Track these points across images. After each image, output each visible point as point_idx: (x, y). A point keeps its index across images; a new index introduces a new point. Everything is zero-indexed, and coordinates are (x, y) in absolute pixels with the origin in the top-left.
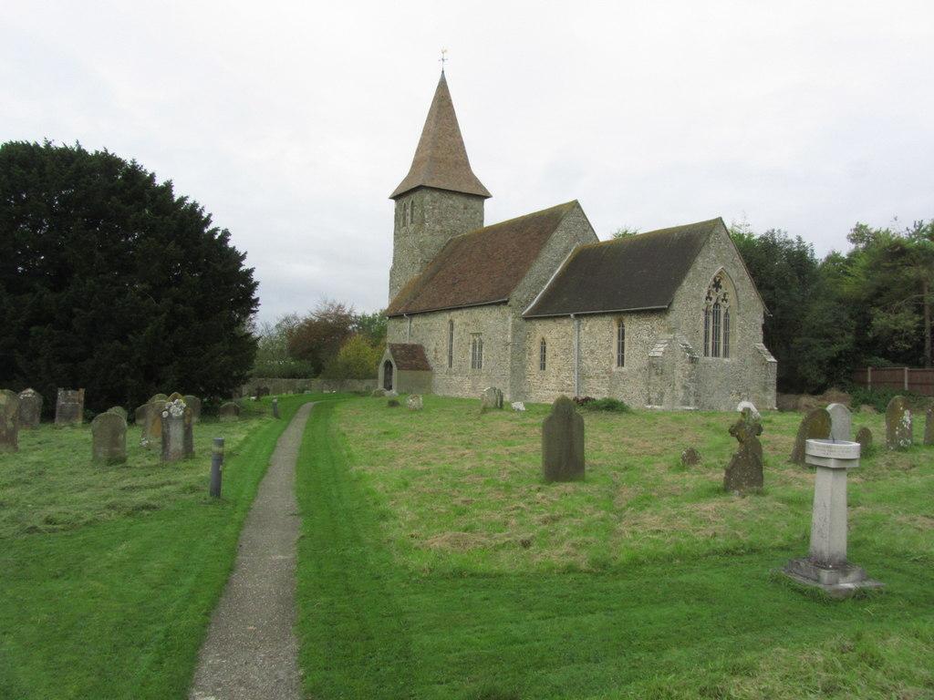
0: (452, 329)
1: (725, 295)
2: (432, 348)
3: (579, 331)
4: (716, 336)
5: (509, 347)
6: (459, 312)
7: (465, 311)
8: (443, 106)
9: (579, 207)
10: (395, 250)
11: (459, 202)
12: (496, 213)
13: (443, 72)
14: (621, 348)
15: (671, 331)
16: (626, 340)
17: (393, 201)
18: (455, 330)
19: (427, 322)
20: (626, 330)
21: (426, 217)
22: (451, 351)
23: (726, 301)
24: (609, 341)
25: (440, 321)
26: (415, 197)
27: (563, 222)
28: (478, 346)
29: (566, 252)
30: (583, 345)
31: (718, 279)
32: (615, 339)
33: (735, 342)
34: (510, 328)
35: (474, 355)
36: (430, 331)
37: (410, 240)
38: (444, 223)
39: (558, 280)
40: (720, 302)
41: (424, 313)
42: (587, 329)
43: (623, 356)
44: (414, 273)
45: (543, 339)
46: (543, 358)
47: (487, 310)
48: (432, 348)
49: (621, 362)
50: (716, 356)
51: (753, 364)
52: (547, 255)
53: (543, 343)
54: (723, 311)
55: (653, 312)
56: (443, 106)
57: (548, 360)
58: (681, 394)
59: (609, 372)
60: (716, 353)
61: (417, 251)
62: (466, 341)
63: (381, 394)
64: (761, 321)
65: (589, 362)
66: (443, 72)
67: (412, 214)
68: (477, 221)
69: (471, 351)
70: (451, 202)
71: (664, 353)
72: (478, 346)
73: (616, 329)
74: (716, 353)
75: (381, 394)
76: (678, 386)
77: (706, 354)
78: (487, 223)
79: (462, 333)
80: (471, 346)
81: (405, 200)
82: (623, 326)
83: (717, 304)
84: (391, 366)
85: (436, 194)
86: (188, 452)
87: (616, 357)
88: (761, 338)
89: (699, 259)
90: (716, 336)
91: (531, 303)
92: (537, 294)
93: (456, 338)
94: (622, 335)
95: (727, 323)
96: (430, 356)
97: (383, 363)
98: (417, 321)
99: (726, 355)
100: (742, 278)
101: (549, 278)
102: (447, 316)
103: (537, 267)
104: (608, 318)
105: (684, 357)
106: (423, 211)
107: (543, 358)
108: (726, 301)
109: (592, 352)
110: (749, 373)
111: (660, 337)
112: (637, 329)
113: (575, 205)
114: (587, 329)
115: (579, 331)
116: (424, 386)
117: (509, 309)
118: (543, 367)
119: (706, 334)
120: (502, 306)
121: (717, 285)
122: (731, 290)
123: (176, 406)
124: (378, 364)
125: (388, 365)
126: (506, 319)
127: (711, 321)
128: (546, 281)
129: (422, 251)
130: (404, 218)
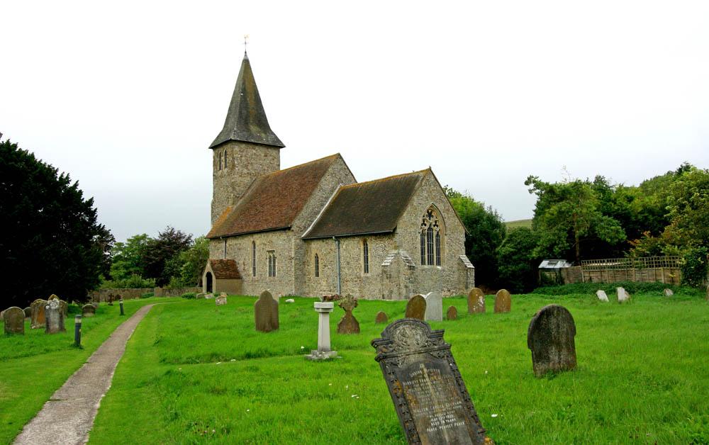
0: (255, 248)
1: (436, 222)
2: (241, 262)
4: (430, 251)
5: (293, 261)
6: (259, 235)
7: (263, 235)
8: (246, 63)
9: (341, 158)
10: (214, 188)
11: (260, 151)
12: (289, 159)
15: (396, 248)
16: (369, 254)
17: (212, 150)
18: (257, 248)
19: (237, 242)
22: (254, 265)
25: (246, 242)
26: (228, 148)
28: (272, 260)
29: (332, 191)
32: (362, 253)
33: (445, 253)
34: (293, 247)
35: (270, 266)
36: (240, 249)
38: (250, 167)
40: (432, 227)
41: (236, 236)
42: (344, 247)
44: (231, 207)
46: (317, 268)
47: (278, 234)
48: (241, 262)
49: (366, 270)
50: (431, 264)
52: (318, 194)
53: (317, 257)
54: (435, 233)
56: (246, 63)
57: (320, 270)
61: (230, 189)
62: (264, 256)
64: (463, 239)
65: (346, 270)
67: (226, 160)
68: (274, 165)
69: (268, 263)
70: (254, 151)
72: (272, 260)
73: (362, 247)
74: (431, 262)
77: (423, 263)
78: (282, 168)
80: (268, 260)
81: (220, 150)
83: (430, 229)
84: (211, 276)
85: (243, 146)
86: (62, 329)
87: (363, 266)
88: (464, 251)
89: (415, 198)
90: (430, 251)
94: (366, 251)
95: (438, 241)
96: (240, 268)
98: (231, 242)
99: (439, 263)
100: (448, 210)
103: (313, 202)
104: (357, 239)
105: (405, 265)
106: (233, 158)
107: (317, 268)
108: (437, 226)
109: (348, 263)
112: (373, 245)
113: (339, 156)
114: (344, 247)
115: (339, 248)
118: (317, 275)
120: (287, 231)
121: (430, 215)
122: (440, 218)
123: (54, 303)
124: (201, 274)
125: (209, 275)
126: (290, 240)
127: (426, 241)
128: (320, 212)
129: (234, 189)
130: (220, 163)
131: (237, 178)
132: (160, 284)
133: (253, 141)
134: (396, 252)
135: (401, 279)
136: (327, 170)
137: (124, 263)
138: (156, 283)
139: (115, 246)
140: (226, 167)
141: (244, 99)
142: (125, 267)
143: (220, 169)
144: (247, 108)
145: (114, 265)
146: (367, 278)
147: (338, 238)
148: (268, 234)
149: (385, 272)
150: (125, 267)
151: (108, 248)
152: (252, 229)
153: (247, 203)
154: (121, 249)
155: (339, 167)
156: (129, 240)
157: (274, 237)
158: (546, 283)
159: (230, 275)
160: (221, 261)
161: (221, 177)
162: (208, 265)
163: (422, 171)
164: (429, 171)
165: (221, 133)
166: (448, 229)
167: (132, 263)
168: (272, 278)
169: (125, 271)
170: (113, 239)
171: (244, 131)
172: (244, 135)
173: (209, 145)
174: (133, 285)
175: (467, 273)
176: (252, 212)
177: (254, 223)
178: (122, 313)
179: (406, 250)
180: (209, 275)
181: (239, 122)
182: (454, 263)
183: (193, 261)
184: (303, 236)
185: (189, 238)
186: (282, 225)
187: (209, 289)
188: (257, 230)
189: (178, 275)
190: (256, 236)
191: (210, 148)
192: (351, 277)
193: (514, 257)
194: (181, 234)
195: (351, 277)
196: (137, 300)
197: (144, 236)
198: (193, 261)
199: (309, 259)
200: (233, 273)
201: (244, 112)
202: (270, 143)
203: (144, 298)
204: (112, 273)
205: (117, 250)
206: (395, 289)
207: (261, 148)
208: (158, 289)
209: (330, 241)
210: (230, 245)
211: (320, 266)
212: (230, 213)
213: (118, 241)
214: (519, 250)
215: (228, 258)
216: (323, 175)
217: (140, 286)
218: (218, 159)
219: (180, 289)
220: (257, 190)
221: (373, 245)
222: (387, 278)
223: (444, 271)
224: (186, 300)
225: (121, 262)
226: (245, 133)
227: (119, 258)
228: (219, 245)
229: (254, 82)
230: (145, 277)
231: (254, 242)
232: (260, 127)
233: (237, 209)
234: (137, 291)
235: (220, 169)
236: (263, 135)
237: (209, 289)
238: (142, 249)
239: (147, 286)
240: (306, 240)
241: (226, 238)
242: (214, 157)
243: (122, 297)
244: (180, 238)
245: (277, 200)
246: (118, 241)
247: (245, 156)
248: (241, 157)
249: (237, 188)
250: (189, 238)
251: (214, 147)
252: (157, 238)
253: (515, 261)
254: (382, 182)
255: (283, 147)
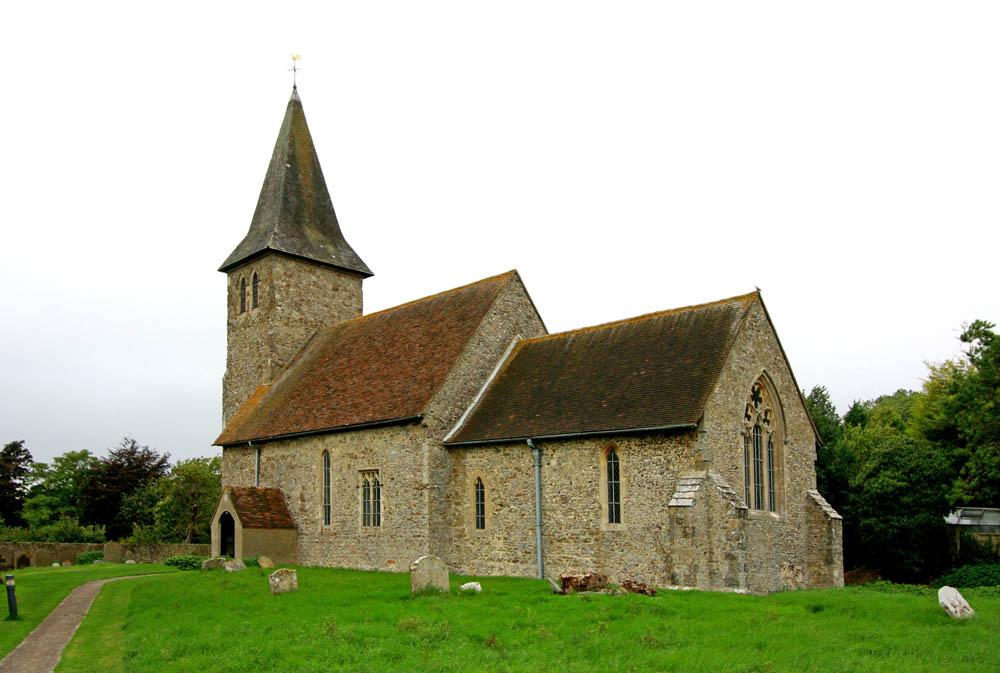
0: (328, 463)
2: (296, 494)
3: (540, 466)
5: (426, 492)
6: (340, 437)
7: (348, 436)
8: (295, 108)
9: (519, 280)
10: (230, 349)
11: (325, 279)
12: (378, 297)
13: (295, 87)
14: (614, 493)
15: (701, 465)
16: (622, 480)
17: (225, 275)
18: (334, 465)
20: (622, 465)
21: (277, 296)
22: (327, 499)
23: (768, 422)
24: (594, 482)
25: (308, 454)
26: (261, 268)
27: (498, 302)
28: (372, 492)
30: (548, 490)
31: (756, 387)
34: (425, 462)
35: (366, 505)
37: (254, 334)
38: (304, 308)
39: (495, 389)
40: (761, 423)
41: (283, 440)
42: (554, 463)
43: (618, 507)
44: (267, 384)
45: (479, 479)
46: (481, 509)
47: (386, 434)
48: (296, 494)
49: (615, 516)
50: (759, 509)
51: (808, 521)
52: (475, 352)
54: (765, 438)
55: (668, 434)
56: (295, 108)
58: (724, 568)
59: (595, 532)
60: (759, 505)
61: (265, 349)
62: (352, 482)
63: (217, 566)
65: (559, 516)
66: (295, 87)
67: (255, 293)
69: (360, 498)
70: (314, 278)
71: (695, 500)
72: (372, 492)
73: (603, 463)
75: (217, 566)
76: (718, 554)
78: (366, 312)
79: (345, 471)
80: (361, 490)
81: (244, 273)
82: (616, 458)
83: (757, 427)
85: (292, 265)
87: (605, 507)
89: (733, 353)
91: (455, 423)
92: (464, 410)
93: (334, 478)
94: (614, 473)
96: (294, 506)
97: (217, 517)
99: (772, 508)
101: (482, 385)
102: (319, 445)
103: (465, 367)
104: (589, 445)
105: (728, 506)
106: (272, 287)
107: (481, 509)
110: (802, 536)
111: (684, 474)
112: (630, 458)
113: (514, 277)
114: (554, 463)
115: (540, 466)
116: (287, 555)
117: (422, 431)
118: (481, 524)
119: (747, 469)
120: (410, 426)
122: (775, 406)
125: (227, 521)
126: (418, 447)
128: (478, 390)
130: (243, 300)
131: (282, 330)
132: (113, 535)
133: (311, 256)
134: (702, 474)
135: (714, 539)
136: (490, 304)
137: (48, 499)
138: (106, 535)
139: (31, 469)
140: (255, 306)
141: (293, 174)
142: (51, 506)
143: (243, 311)
144: (298, 194)
145: (29, 501)
146: (619, 534)
147: (539, 443)
148: (361, 434)
149: (679, 521)
150: (51, 506)
151: (20, 472)
152: (321, 425)
153: (304, 376)
154: (43, 475)
155: (517, 299)
156: (57, 460)
157: (376, 441)
158: (981, 556)
159: (272, 519)
160: (253, 491)
161: (246, 325)
162: (226, 498)
163: (736, 299)
164: (756, 298)
165: (243, 242)
166: (789, 431)
167: (62, 500)
168: (371, 529)
169: (50, 512)
170: (28, 457)
171: (293, 236)
172: (294, 245)
173: (220, 264)
174: (62, 537)
175: (829, 531)
176: (319, 392)
177: (328, 413)
178: (13, 614)
179: (719, 472)
180: (227, 521)
181: (283, 218)
182: (800, 504)
183: (177, 494)
184: (445, 439)
185: (164, 460)
186: (402, 415)
187: (227, 548)
188: (334, 424)
189: (149, 520)
190: (331, 440)
191: (221, 270)
192: (572, 530)
193: (906, 499)
194: (150, 453)
195: (572, 530)
196: (68, 568)
197: (84, 455)
198: (177, 494)
199: (459, 489)
200: (279, 517)
201: (293, 199)
202: (345, 264)
203: (82, 562)
204: (26, 515)
205: (36, 476)
206: (703, 562)
207: (327, 272)
208: (111, 547)
209: (516, 451)
210: (269, 459)
211: (489, 505)
212: (267, 395)
213: (36, 459)
214: (914, 484)
215: (264, 485)
216: (485, 312)
217: (75, 538)
218: (238, 292)
219: (153, 546)
220: (323, 350)
221: (635, 460)
222: (686, 535)
223: (783, 522)
224: (179, 574)
225: (42, 497)
226: (294, 239)
227: (36, 490)
228: (243, 460)
229: (311, 145)
230: (84, 522)
231: (326, 453)
232: (324, 233)
233: (278, 392)
234: (65, 548)
235: (243, 311)
236: (331, 249)
237: (227, 548)
238: (79, 477)
239: (90, 540)
240: (450, 447)
241: (260, 444)
242: (229, 289)
243: (32, 561)
244: (148, 459)
245: (374, 367)
246: (36, 459)
247: (296, 286)
248: (288, 286)
249: (279, 347)
250: (164, 460)
251: (227, 269)
252: (107, 458)
253: (907, 506)
254: (591, 336)
255: (368, 275)
